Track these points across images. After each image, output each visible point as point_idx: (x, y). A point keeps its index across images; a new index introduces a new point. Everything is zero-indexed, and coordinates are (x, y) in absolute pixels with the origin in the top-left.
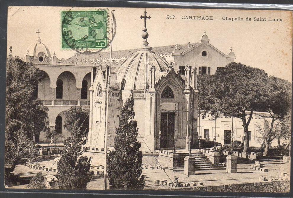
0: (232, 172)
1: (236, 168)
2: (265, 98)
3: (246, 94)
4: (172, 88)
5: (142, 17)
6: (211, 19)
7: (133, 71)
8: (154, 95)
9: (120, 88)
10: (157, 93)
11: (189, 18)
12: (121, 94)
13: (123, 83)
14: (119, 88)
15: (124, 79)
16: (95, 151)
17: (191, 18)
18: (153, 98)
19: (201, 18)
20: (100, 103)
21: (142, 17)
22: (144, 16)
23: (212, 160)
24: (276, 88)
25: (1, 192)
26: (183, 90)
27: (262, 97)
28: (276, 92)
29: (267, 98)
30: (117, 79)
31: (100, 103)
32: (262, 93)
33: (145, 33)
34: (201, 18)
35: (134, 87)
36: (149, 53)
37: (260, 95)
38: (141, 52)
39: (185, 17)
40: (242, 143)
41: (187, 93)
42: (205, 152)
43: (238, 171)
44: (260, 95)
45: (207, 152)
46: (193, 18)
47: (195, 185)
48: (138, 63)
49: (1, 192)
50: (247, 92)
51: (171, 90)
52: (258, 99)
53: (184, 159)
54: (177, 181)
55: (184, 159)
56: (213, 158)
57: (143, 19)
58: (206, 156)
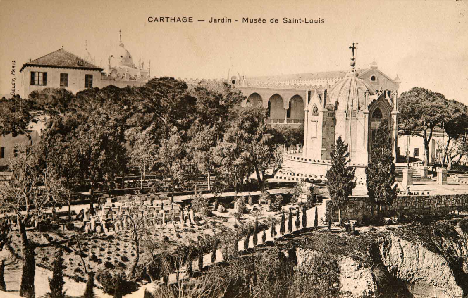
0: (443, 183)
1: (446, 180)
2: (449, 119)
3: (431, 116)
4: (381, 110)
5: (350, 48)
6: (190, 21)
7: (345, 93)
8: (367, 115)
9: (334, 109)
10: (369, 114)
11: (159, 20)
12: (335, 114)
13: (337, 105)
14: (332, 109)
15: (337, 102)
16: (304, 161)
17: (161, 21)
18: (367, 118)
19: (176, 19)
20: (316, 121)
21: (350, 48)
22: (352, 46)
23: (422, 173)
24: (457, 111)
25: (466, 213)
26: (391, 111)
27: (445, 119)
28: (457, 115)
29: (450, 119)
30: (330, 101)
31: (316, 121)
32: (446, 114)
33: (353, 62)
34: (176, 19)
35: (347, 109)
36: (357, 79)
37: (444, 117)
38: (350, 78)
39: (154, 19)
40: (178, 132)
41: (394, 114)
42: (414, 165)
43: (448, 183)
44: (444, 117)
45: (416, 165)
46: (165, 19)
47: (423, 194)
48: (349, 88)
49: (466, 213)
50: (433, 113)
51: (380, 111)
52: (442, 120)
53: (403, 171)
54: (409, 190)
55: (403, 171)
56: (423, 171)
57: (351, 49)
58: (414, 169)
